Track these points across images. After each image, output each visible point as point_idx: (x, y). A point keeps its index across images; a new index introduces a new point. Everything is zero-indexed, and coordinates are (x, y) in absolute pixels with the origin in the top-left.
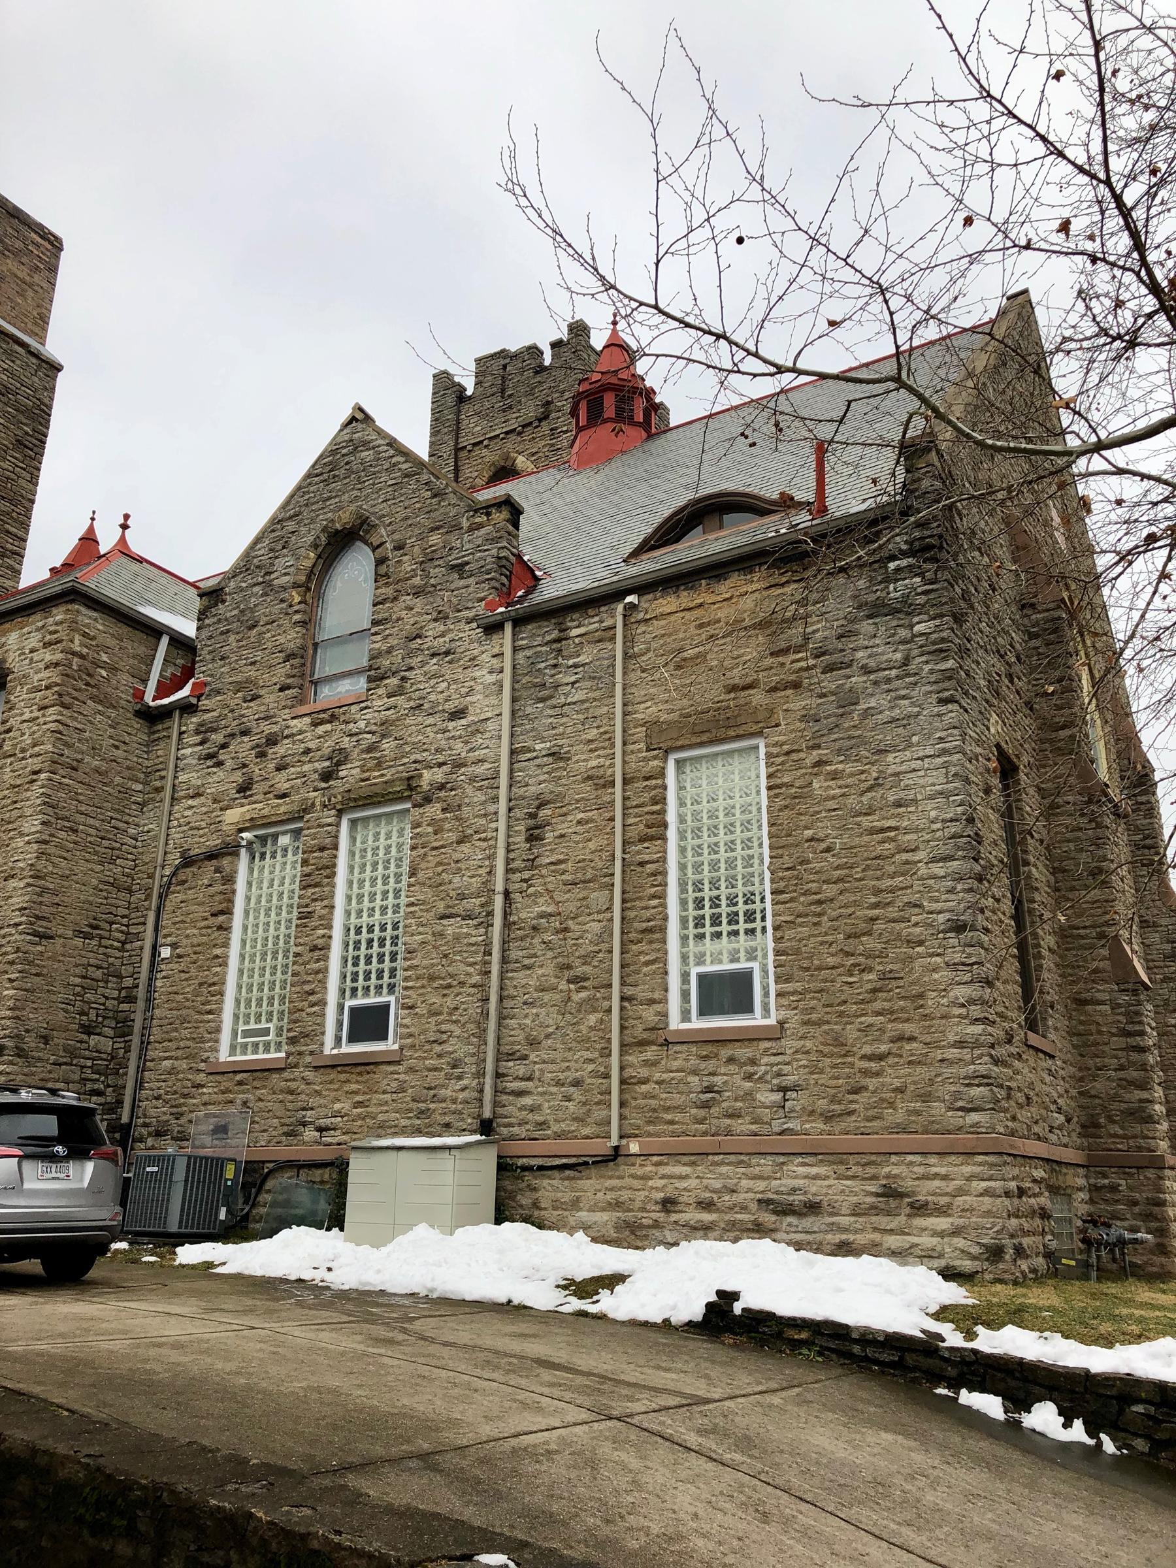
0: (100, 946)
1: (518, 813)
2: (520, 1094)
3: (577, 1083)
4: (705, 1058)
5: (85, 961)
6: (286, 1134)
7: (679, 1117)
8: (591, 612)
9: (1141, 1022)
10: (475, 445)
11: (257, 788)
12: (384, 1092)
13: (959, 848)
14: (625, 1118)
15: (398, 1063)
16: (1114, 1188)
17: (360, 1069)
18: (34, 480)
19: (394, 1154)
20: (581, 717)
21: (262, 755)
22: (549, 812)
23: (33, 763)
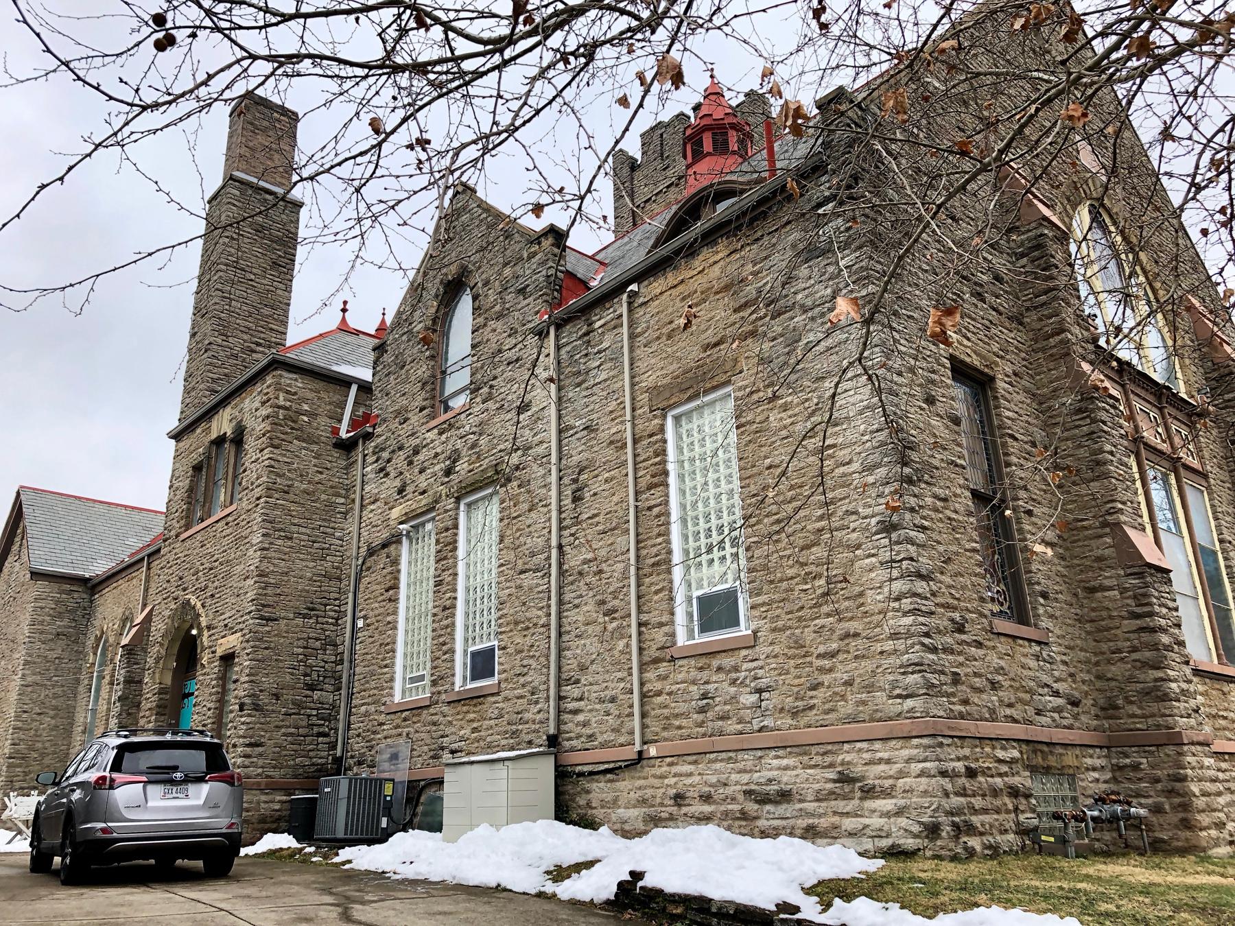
0: (317, 623)
1: (566, 480)
2: (576, 712)
3: (613, 700)
4: (701, 669)
5: (305, 635)
6: (433, 757)
7: (684, 722)
8: (607, 305)
9: (1151, 604)
10: (646, 202)
11: (410, 489)
12: (491, 719)
13: (886, 455)
14: (648, 727)
15: (498, 694)
16: (1136, 767)
17: (475, 701)
18: (288, 289)
19: (468, 767)
20: (605, 393)
21: (410, 463)
22: (586, 476)
23: (258, 492)
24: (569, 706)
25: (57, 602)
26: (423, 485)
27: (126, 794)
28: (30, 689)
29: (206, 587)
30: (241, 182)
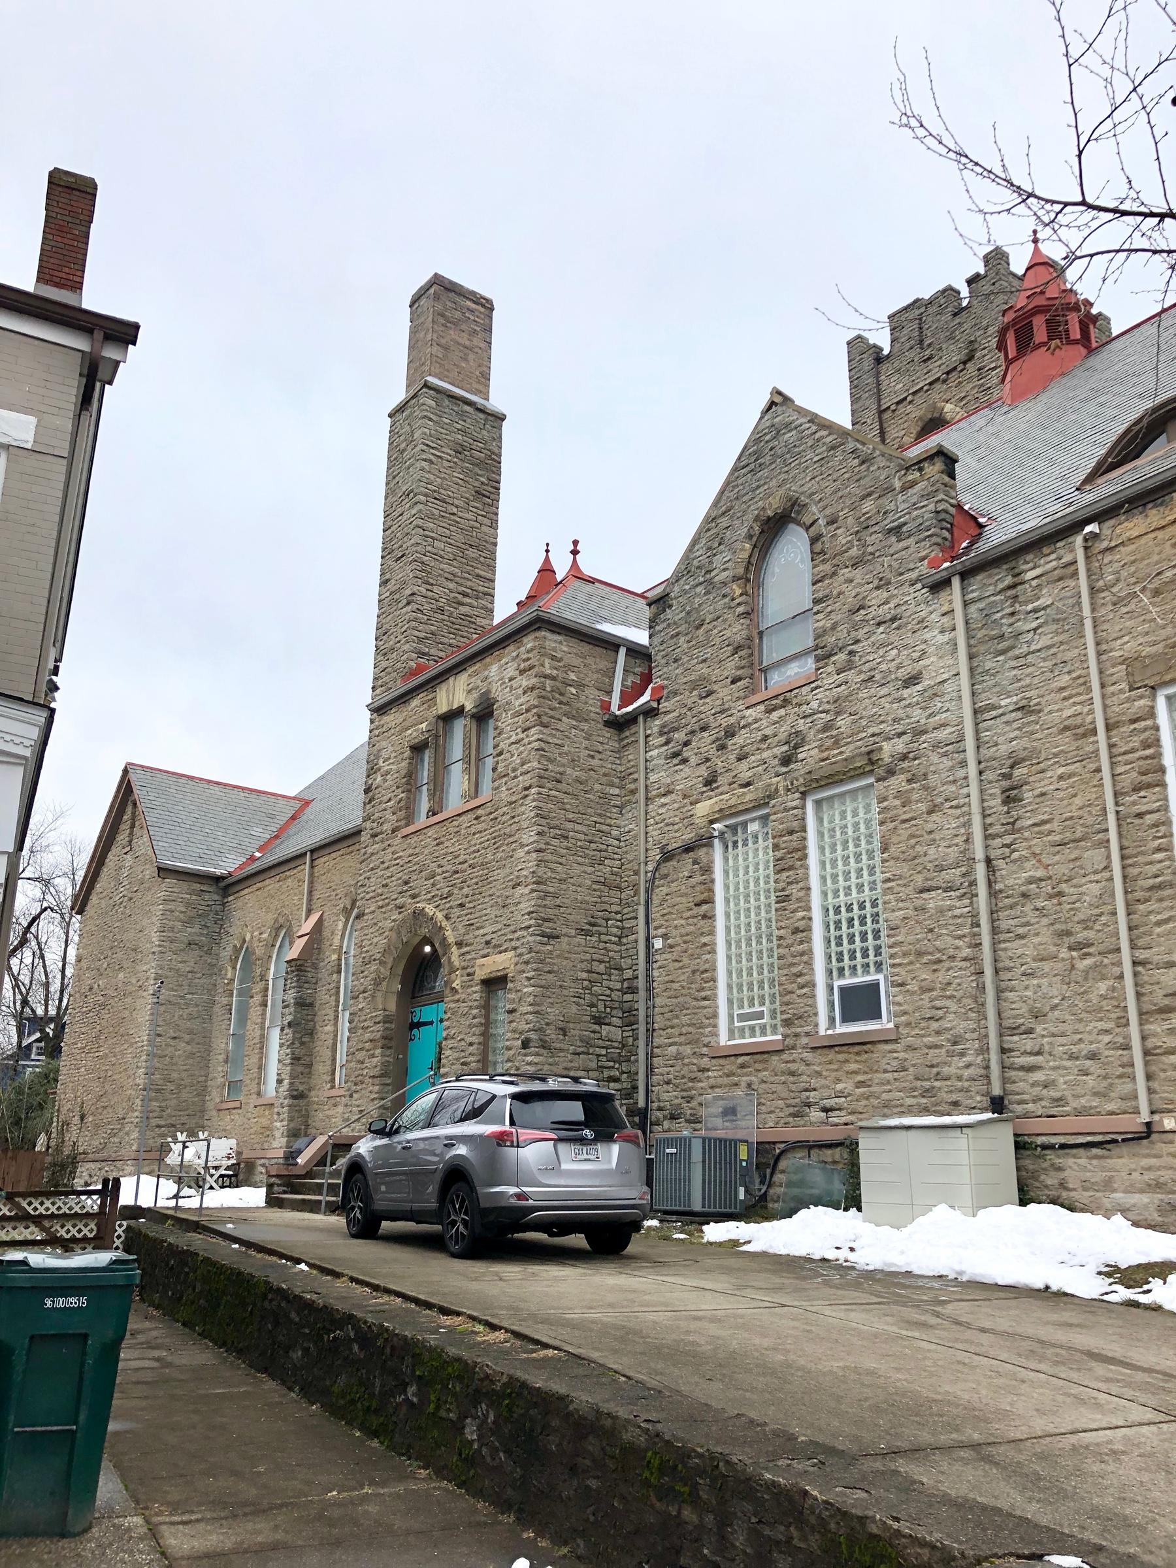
3: (1093, 1056)
5: (588, 957)
8: (1046, 550)
10: (898, 403)
11: (722, 780)
12: (885, 1071)
15: (896, 1041)
17: (857, 1048)
18: (494, 525)
20: (1049, 664)
22: (1025, 771)
23: (524, 780)
24: (1017, 1060)
25: (188, 904)
26: (746, 775)
27: (533, 1153)
28: (163, 1008)
29: (450, 895)
30: (437, 390)
